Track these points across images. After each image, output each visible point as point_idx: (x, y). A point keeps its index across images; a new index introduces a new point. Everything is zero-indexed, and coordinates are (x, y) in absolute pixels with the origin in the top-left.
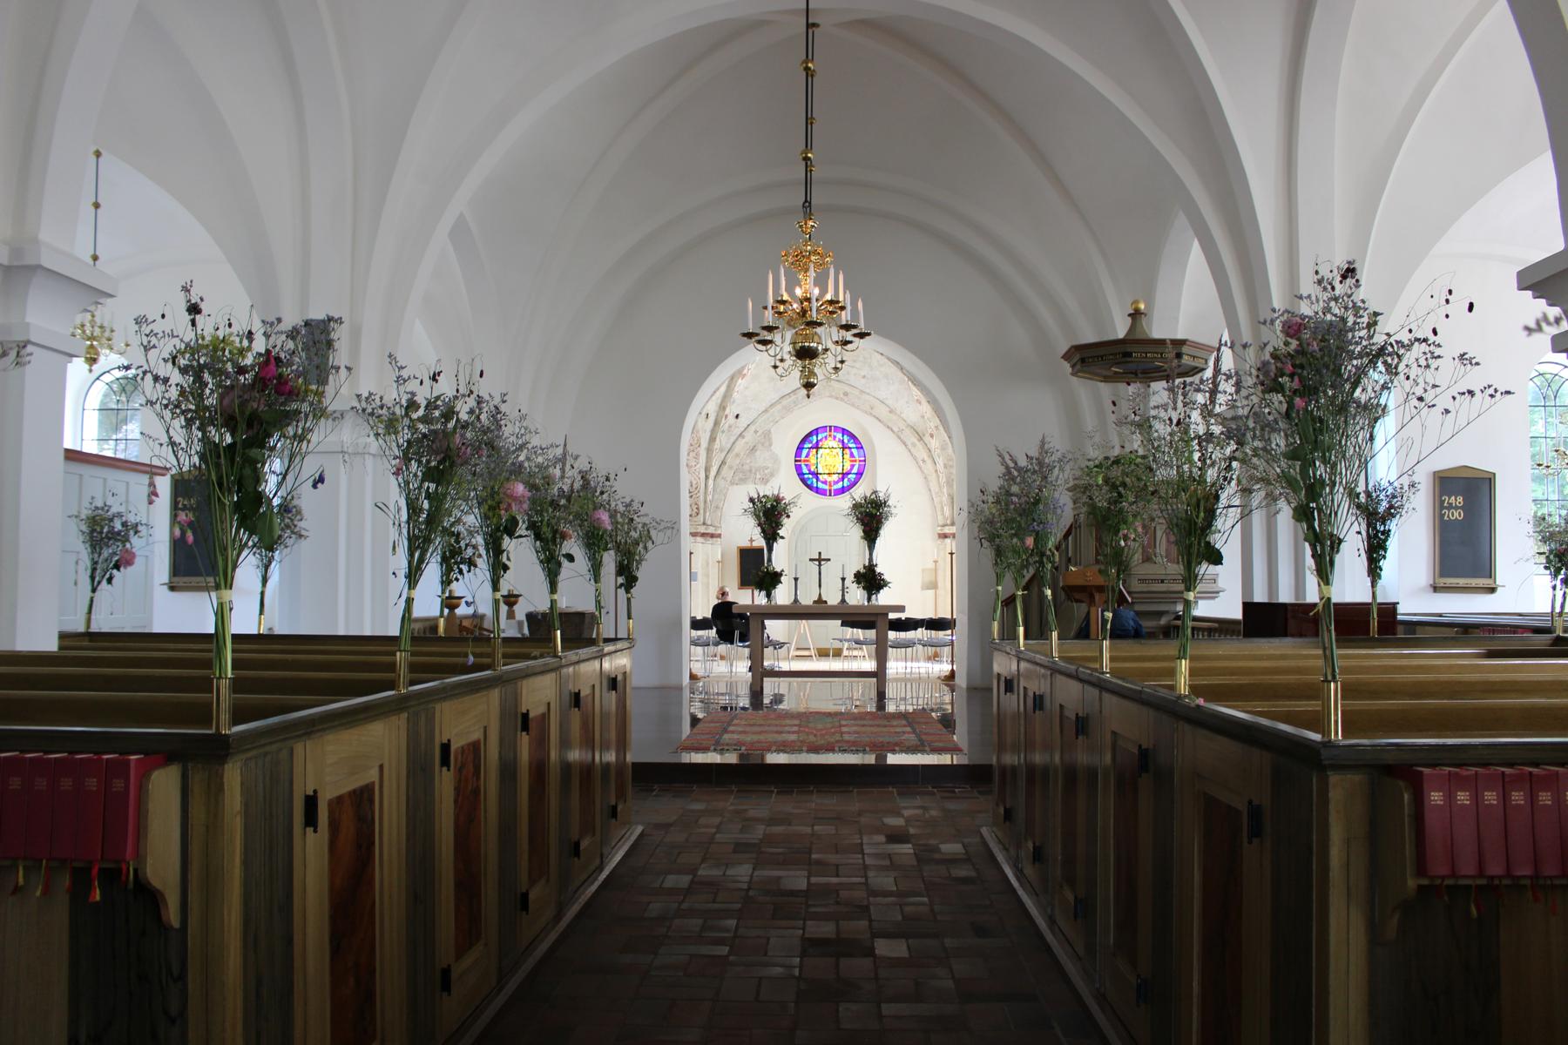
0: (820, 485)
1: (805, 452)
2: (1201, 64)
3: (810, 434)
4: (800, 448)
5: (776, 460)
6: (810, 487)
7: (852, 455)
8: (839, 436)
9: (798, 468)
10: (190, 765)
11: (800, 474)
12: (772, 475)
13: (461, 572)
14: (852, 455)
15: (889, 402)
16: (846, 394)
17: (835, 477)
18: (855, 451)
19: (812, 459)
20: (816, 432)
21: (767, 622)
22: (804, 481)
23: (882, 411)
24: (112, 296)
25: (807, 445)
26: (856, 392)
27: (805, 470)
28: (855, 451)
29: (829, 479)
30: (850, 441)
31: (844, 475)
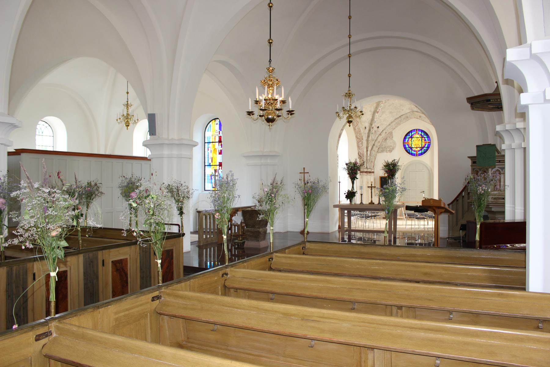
0: (413, 152)
1: (407, 140)
3: (409, 133)
4: (405, 138)
5: (394, 143)
6: (409, 153)
8: (420, 133)
12: (393, 149)
14: (425, 140)
16: (420, 117)
17: (419, 149)
18: (426, 139)
19: (410, 142)
20: (411, 131)
22: (407, 151)
27: (407, 147)
28: (426, 139)
31: (422, 148)
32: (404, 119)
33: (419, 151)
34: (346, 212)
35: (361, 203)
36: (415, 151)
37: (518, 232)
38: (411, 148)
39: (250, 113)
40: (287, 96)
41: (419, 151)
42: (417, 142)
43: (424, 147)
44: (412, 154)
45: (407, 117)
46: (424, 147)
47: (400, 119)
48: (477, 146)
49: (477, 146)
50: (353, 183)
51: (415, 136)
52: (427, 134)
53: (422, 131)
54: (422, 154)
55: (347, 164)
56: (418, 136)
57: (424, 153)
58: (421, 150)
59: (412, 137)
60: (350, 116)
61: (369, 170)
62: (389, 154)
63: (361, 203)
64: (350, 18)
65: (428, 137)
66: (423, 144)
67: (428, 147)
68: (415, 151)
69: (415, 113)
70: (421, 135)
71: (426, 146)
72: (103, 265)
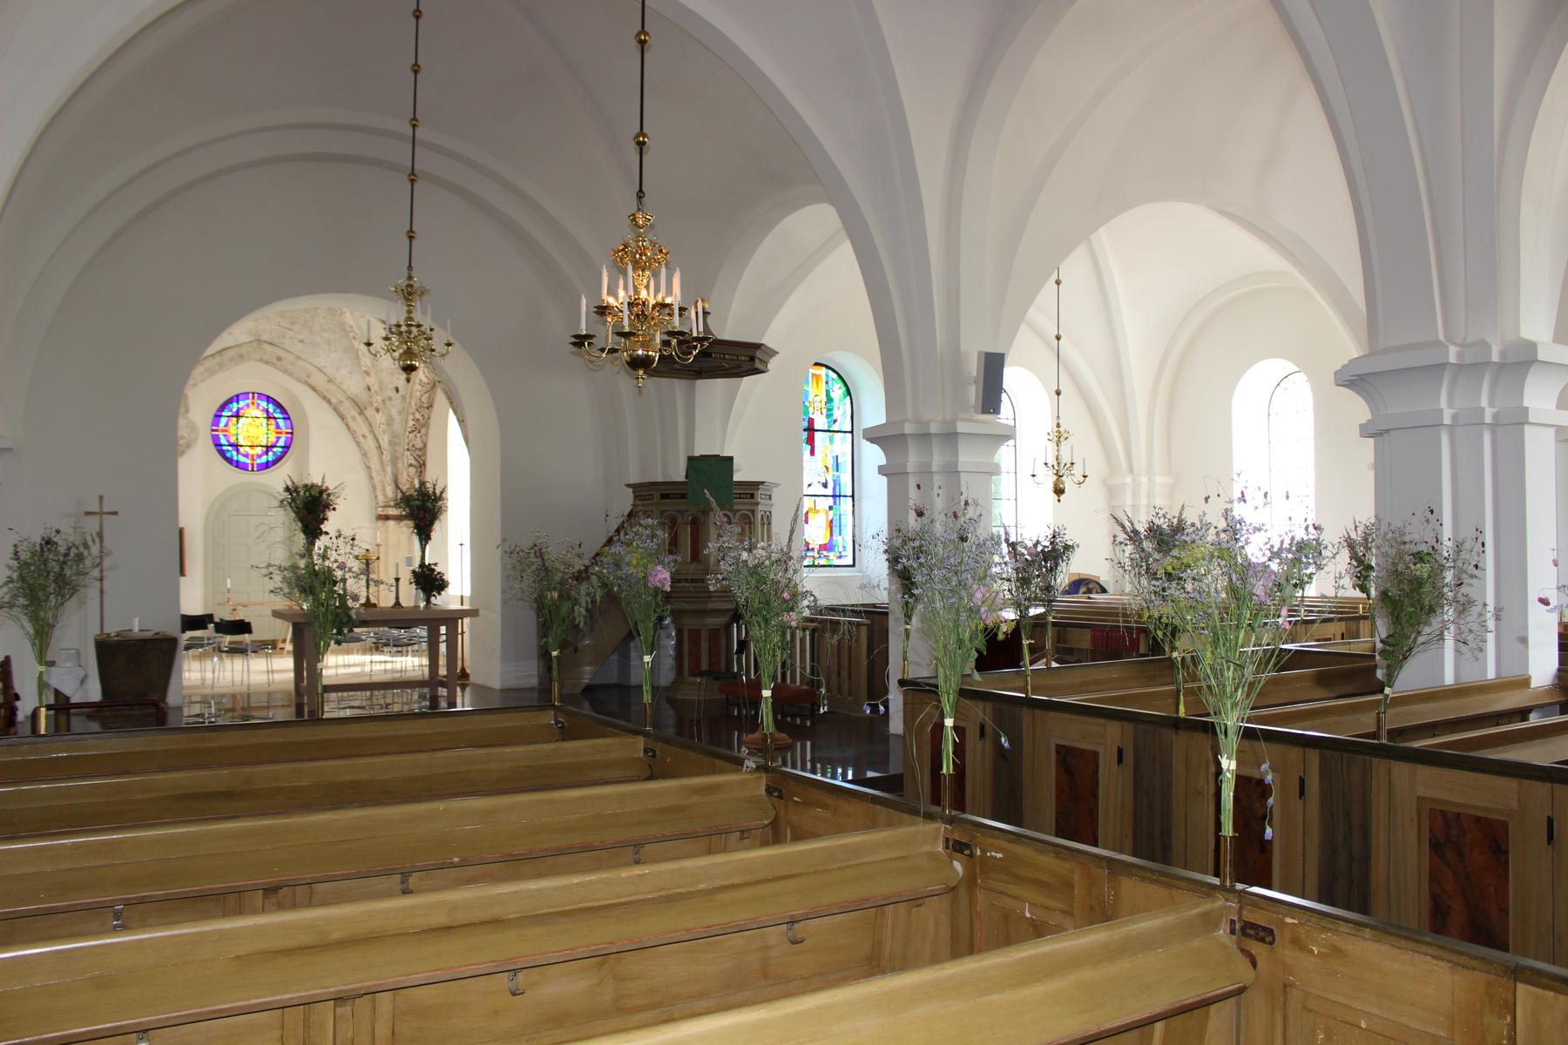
0: (242, 459)
3: (230, 401)
5: (193, 428)
6: (230, 461)
7: (278, 426)
9: (216, 440)
11: (218, 445)
14: (278, 426)
15: (329, 371)
16: (279, 359)
17: (258, 450)
18: (281, 422)
19: (232, 429)
20: (237, 398)
22: (222, 453)
23: (319, 381)
26: (292, 358)
27: (223, 441)
28: (281, 422)
30: (278, 409)
31: (268, 448)
32: (231, 360)
33: (259, 456)
34: (443, 629)
35: (397, 603)
36: (246, 456)
37: (1506, 853)
38: (236, 446)
39: (580, 341)
41: (259, 456)
42: (253, 431)
44: (238, 465)
45: (241, 356)
47: (218, 359)
48: (731, 459)
49: (731, 459)
53: (269, 399)
54: (267, 465)
57: (275, 462)
59: (237, 415)
60: (409, 353)
63: (397, 603)
64: (416, 69)
67: (286, 448)
68: (246, 456)
69: (266, 346)
70: (267, 411)
71: (281, 443)
72: (1302, 782)
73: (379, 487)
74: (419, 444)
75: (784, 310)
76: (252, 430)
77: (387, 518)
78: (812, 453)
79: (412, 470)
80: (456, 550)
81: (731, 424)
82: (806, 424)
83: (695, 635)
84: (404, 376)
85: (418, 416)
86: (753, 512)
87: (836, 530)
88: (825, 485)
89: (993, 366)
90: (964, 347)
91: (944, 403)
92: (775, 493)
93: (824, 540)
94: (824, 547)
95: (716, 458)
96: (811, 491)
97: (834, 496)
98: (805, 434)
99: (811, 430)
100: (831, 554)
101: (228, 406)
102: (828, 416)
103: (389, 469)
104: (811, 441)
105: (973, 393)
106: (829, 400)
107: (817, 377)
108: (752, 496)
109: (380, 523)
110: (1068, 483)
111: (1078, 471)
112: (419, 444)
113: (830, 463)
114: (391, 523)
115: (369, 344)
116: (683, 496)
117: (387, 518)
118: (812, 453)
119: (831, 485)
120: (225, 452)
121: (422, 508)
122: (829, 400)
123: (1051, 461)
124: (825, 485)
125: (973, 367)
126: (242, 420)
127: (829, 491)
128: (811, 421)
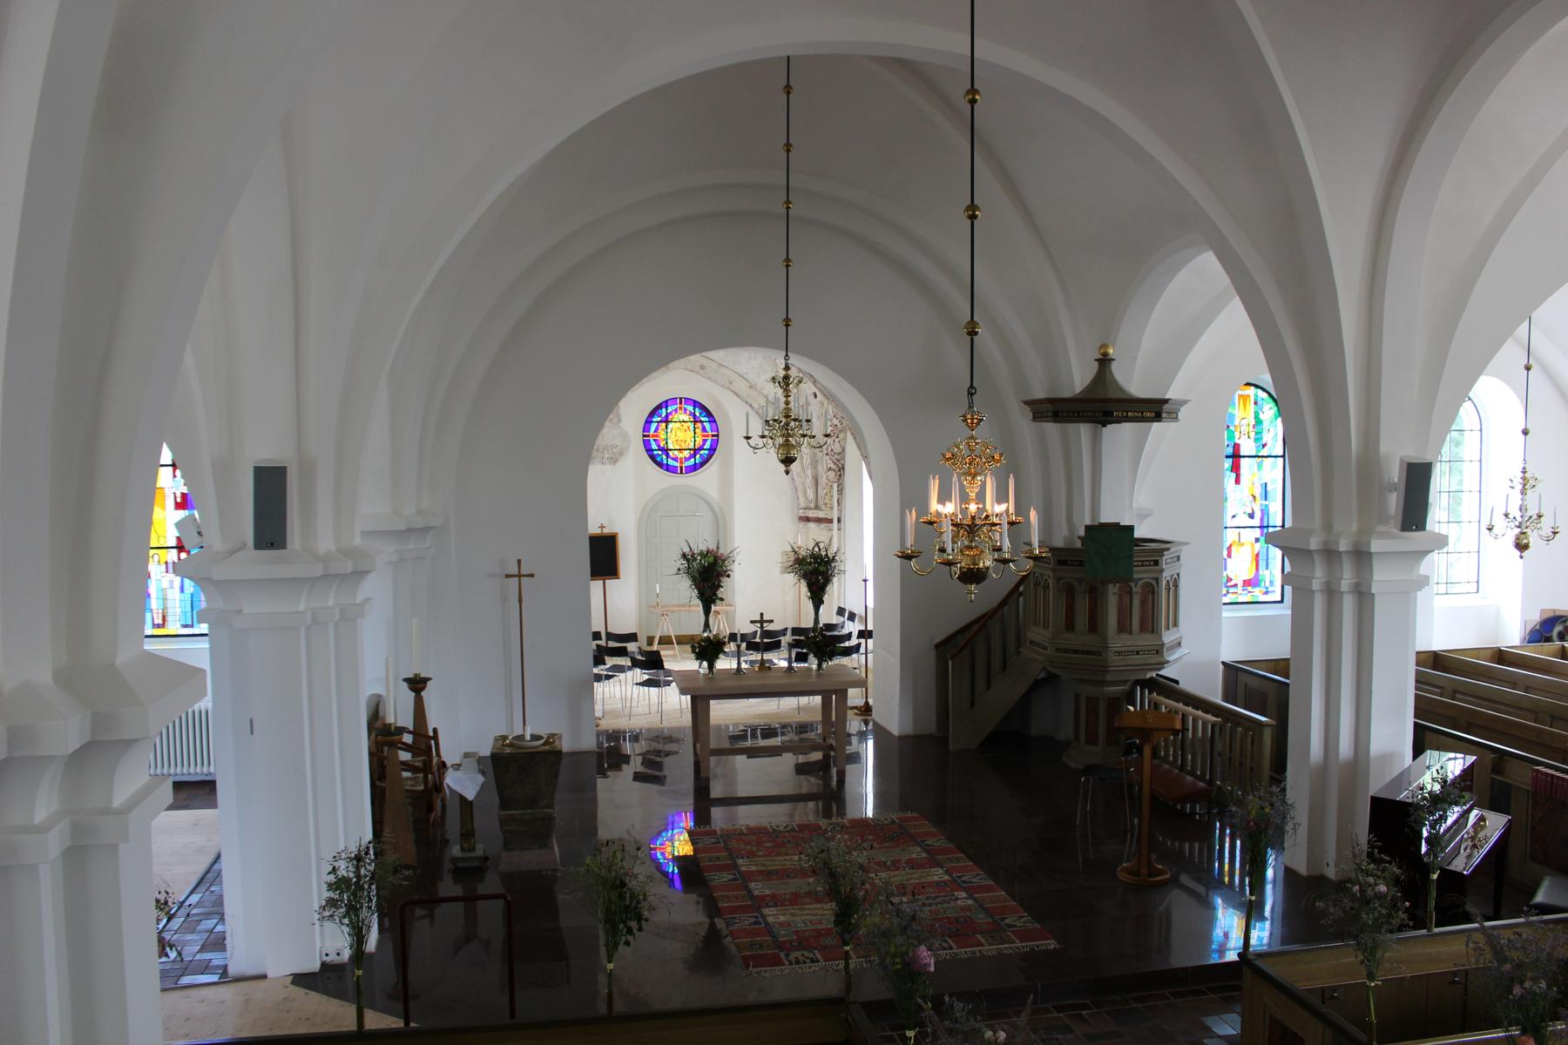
0: (671, 462)
1: (654, 426)
2: (1257, 45)
3: (659, 407)
4: (648, 422)
5: (624, 436)
6: (660, 464)
7: (704, 429)
8: (690, 408)
9: (647, 444)
10: (354, 1028)
11: (649, 450)
12: (621, 454)
13: (630, 931)
14: (704, 429)
15: (750, 377)
16: (702, 367)
17: (686, 454)
18: (707, 426)
19: (662, 435)
20: (665, 404)
21: (712, 702)
22: (653, 458)
23: (741, 386)
24: (218, 857)
25: (656, 419)
26: (714, 366)
27: (654, 446)
28: (707, 426)
29: (680, 455)
30: (703, 413)
31: (696, 451)
33: (687, 459)
36: (675, 459)
38: (666, 451)
40: (1020, 508)
41: (687, 459)
42: (681, 435)
43: (701, 448)
44: (668, 468)
46: (701, 448)
50: (707, 611)
51: (676, 417)
52: (709, 414)
53: (696, 404)
54: (695, 468)
55: (684, 556)
56: (686, 418)
57: (702, 464)
58: (694, 456)
59: (666, 421)
61: (821, 515)
62: (608, 467)
65: (713, 421)
66: (699, 440)
67: (713, 450)
68: (675, 459)
71: (707, 446)
73: (800, 488)
74: (837, 449)
75: (1204, 339)
76: (680, 435)
77: (808, 519)
78: (1237, 481)
79: (831, 474)
80: (859, 590)
81: (1138, 484)
82: (1230, 451)
83: (1093, 702)
84: (782, 467)
85: (835, 422)
86: (1157, 580)
87: (1262, 564)
88: (1251, 516)
89: (1418, 478)
90: (1384, 447)
91: (1363, 505)
92: (1185, 554)
93: (1250, 575)
94: (1247, 583)
95: (1116, 526)
96: (1235, 523)
97: (1261, 527)
98: (1228, 463)
99: (1236, 456)
100: (1257, 590)
101: (658, 413)
102: (1256, 440)
103: (809, 472)
104: (1236, 468)
105: (1394, 502)
106: (1258, 422)
107: (1245, 398)
108: (1156, 563)
109: (802, 525)
110: (1533, 539)
111: (1546, 526)
112: (837, 449)
113: (1258, 492)
114: (812, 525)
115: (748, 438)
116: (1081, 563)
117: (808, 519)
118: (1237, 481)
119: (1258, 515)
120: (658, 456)
121: (816, 572)
122: (1258, 422)
123: (1515, 512)
124: (1251, 516)
125: (1395, 474)
126: (671, 425)
127: (1256, 522)
128: (1237, 447)
